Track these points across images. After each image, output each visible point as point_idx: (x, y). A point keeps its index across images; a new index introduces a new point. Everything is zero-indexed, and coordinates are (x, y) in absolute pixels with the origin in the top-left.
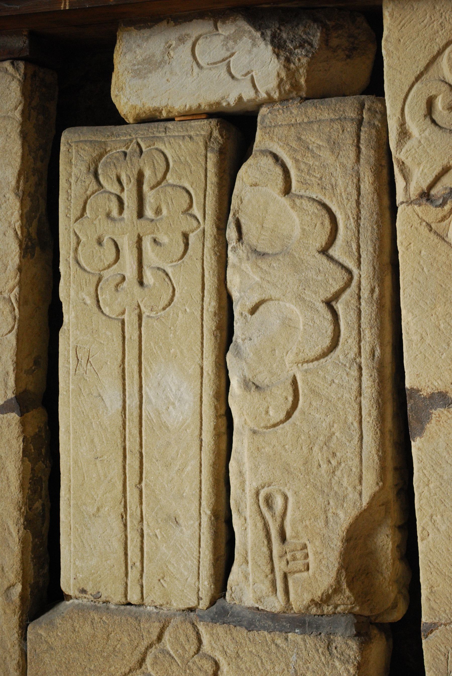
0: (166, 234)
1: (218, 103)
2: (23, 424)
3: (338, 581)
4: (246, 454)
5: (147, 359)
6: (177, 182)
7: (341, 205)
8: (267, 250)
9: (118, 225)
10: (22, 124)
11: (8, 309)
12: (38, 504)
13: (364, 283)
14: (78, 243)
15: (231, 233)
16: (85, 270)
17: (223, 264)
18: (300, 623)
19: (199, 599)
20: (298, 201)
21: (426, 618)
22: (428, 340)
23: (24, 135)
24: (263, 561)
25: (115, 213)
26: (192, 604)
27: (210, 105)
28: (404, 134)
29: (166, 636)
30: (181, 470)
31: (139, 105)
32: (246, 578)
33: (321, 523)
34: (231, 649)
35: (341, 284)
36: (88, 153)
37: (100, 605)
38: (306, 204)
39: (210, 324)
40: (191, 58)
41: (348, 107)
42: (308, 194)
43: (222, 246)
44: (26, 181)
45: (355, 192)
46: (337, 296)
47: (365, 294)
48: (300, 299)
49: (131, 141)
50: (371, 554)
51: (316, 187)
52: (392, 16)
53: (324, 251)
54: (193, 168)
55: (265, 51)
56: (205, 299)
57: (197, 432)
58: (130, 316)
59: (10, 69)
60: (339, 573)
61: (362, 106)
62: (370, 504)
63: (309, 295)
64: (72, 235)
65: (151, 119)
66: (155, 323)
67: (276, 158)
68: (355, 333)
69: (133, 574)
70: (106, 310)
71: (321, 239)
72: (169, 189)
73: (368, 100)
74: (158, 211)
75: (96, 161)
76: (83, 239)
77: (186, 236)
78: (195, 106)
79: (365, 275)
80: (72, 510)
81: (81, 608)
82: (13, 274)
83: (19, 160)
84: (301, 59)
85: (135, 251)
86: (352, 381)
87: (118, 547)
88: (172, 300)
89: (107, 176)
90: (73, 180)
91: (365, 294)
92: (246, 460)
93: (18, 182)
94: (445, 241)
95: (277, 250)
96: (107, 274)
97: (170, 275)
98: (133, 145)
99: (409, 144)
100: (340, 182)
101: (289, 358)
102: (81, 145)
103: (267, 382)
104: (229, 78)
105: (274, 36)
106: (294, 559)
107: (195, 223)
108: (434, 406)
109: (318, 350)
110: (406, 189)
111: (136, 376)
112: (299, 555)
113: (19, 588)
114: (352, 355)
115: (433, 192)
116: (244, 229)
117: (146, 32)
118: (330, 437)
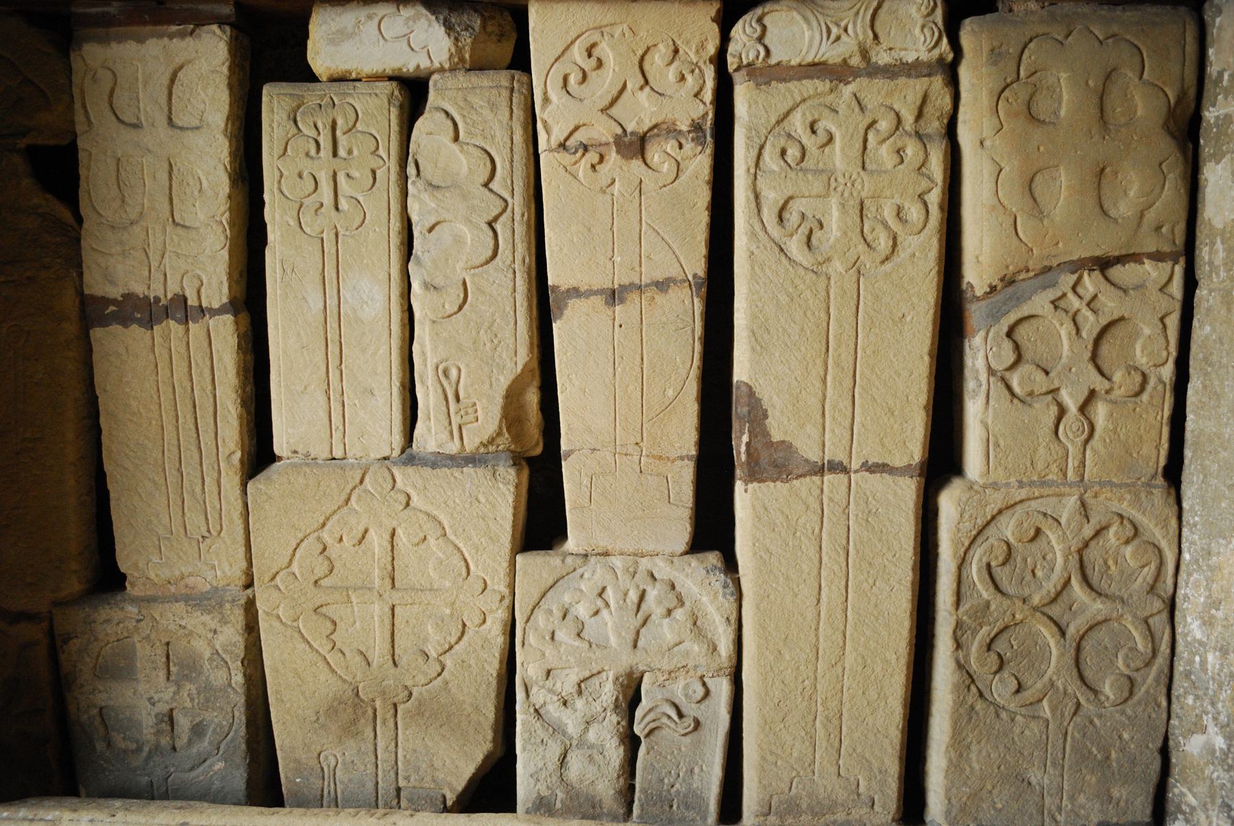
2: (236, 323)
3: (500, 428)
4: (427, 338)
9: (316, 162)
10: (229, 78)
11: (220, 229)
12: (248, 389)
14: (281, 176)
15: (411, 170)
17: (405, 194)
18: (472, 460)
19: (392, 449)
20: (465, 147)
21: (564, 447)
22: (565, 251)
23: (231, 87)
24: (443, 417)
25: (313, 152)
26: (386, 454)
28: (546, 100)
29: (367, 479)
30: (375, 353)
31: (333, 67)
32: (429, 430)
33: (487, 386)
34: (420, 483)
36: (288, 104)
37: (311, 461)
39: (395, 240)
41: (503, 77)
42: (473, 141)
43: (404, 178)
44: (233, 125)
46: (496, 219)
47: (517, 217)
48: (468, 221)
50: (522, 406)
52: (537, 12)
53: (486, 185)
55: (439, 31)
59: (218, 31)
60: (501, 421)
61: (513, 78)
62: (523, 370)
63: (475, 218)
65: (340, 79)
67: (447, 113)
68: (510, 246)
69: (337, 435)
70: (307, 230)
71: (484, 177)
73: (518, 74)
74: (350, 152)
75: (295, 111)
76: (286, 173)
77: (374, 172)
78: (380, 71)
79: (518, 203)
80: (283, 390)
81: (294, 466)
82: (224, 201)
83: (227, 107)
84: (467, 39)
85: (332, 183)
87: (323, 415)
88: (363, 222)
89: (304, 122)
91: (517, 217)
92: (427, 342)
93: (226, 125)
95: (449, 184)
96: (307, 202)
98: (327, 99)
99: (550, 108)
100: (498, 134)
105: (445, 20)
106: (467, 414)
107: (382, 163)
108: (569, 297)
109: (483, 259)
110: (548, 140)
112: (470, 410)
113: (239, 454)
114: (508, 262)
116: (421, 168)
117: (339, 9)
118: (492, 324)
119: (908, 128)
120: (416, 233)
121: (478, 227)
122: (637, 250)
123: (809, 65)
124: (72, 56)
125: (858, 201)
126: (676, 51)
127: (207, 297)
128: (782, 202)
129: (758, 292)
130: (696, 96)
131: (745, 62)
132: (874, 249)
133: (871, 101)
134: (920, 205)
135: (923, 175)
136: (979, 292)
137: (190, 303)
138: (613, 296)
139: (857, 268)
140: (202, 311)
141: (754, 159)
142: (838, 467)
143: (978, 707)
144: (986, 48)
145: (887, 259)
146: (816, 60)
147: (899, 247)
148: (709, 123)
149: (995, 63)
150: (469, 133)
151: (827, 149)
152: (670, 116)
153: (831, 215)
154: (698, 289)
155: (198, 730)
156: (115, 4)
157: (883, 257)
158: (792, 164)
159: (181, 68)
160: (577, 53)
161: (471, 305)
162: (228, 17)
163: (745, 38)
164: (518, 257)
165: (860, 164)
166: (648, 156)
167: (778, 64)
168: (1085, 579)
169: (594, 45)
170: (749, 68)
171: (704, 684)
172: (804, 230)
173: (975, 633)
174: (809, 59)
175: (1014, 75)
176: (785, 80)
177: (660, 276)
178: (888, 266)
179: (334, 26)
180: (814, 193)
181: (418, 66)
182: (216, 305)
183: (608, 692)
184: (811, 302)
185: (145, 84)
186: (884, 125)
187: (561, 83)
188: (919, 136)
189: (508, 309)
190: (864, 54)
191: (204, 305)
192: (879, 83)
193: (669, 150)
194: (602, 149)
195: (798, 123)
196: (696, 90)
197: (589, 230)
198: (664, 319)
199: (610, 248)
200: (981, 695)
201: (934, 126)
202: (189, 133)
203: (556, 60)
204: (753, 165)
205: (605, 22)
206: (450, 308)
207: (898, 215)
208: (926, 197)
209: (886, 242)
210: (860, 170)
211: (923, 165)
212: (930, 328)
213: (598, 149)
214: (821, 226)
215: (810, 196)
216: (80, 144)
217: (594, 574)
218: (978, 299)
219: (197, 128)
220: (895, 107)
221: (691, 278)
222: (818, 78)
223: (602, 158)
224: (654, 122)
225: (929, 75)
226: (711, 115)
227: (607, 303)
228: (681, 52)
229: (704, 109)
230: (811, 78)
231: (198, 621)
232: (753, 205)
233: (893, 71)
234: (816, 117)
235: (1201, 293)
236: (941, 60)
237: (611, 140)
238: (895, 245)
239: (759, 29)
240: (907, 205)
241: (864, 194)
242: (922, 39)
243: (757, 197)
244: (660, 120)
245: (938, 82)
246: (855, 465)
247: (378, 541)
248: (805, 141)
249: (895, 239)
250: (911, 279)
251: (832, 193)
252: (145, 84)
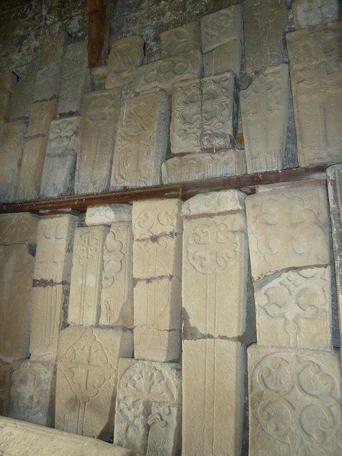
18: (112, 327)
37: (75, 326)
55: (112, 213)
56: (309, 270)
94: (325, 124)
138: (149, 281)
142: (210, 336)
143: (261, 434)
155: (38, 403)
160: (142, 216)
168: (301, 387)
170: (187, 217)
171: (170, 409)
173: (259, 402)
183: (141, 407)
200: (262, 429)
217: (139, 365)
231: (43, 369)
235: (287, 72)
246: (216, 337)
247: (87, 349)
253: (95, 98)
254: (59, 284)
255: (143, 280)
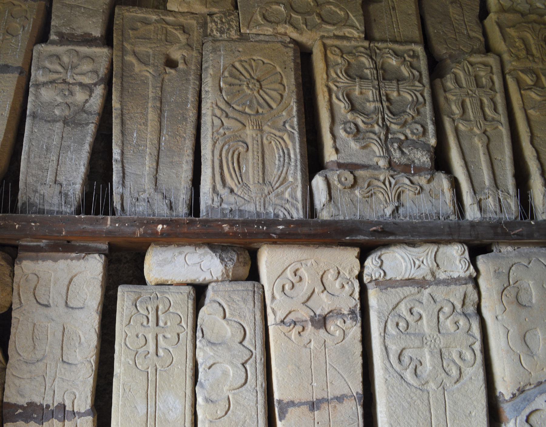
0: (170, 333)
1: (195, 280)
5: (159, 390)
6: (175, 311)
7: (248, 324)
8: (215, 342)
9: (147, 329)
13: (258, 356)
15: (199, 334)
16: (129, 348)
20: (230, 322)
22: (286, 380)
25: (145, 323)
27: (192, 281)
28: (273, 298)
31: (159, 278)
35: (249, 357)
36: (133, 296)
38: (233, 323)
39: (189, 373)
40: (184, 261)
41: (249, 285)
42: (233, 319)
43: (195, 338)
45: (253, 319)
46: (246, 362)
48: (231, 363)
49: (153, 292)
51: (237, 317)
53: (241, 343)
54: (182, 306)
55: (217, 261)
57: (183, 423)
58: (151, 369)
63: (235, 361)
64: (123, 333)
66: (164, 373)
67: (220, 304)
68: (255, 377)
70: (140, 367)
72: (171, 314)
74: (166, 324)
75: (136, 300)
76: (129, 334)
77: (178, 335)
79: (258, 353)
84: (230, 265)
85: (155, 341)
86: (254, 398)
89: (141, 306)
90: (125, 308)
93: (98, 307)
95: (220, 342)
97: (171, 352)
99: (275, 302)
100: (247, 315)
101: (225, 388)
102: (129, 293)
103: (215, 399)
104: (200, 270)
105: (220, 256)
107: (183, 330)
111: (154, 397)
114: (254, 386)
115: (285, 321)
117: (164, 249)
119: (459, 311)
120: (201, 370)
121: (236, 366)
122: (325, 379)
123: (406, 280)
124: (16, 266)
125: (439, 350)
126: (339, 273)
127: (78, 405)
128: (399, 351)
129: (392, 402)
130: (351, 295)
131: (374, 278)
132: (450, 376)
133: (438, 298)
134: (471, 351)
135: (470, 335)
136: (507, 398)
137: (67, 409)
138: (313, 406)
139: (442, 386)
140: (74, 414)
141: (383, 329)
144: (492, 270)
145: (458, 381)
146: (410, 277)
147: (463, 374)
148: (358, 309)
149: (497, 278)
150: (232, 314)
151: (419, 323)
152: (338, 306)
153: (425, 357)
154: (359, 401)
156: (44, 241)
157: (456, 380)
158: (403, 331)
159: (75, 276)
160: (289, 273)
161: (233, 412)
162: (105, 250)
163: (373, 267)
164: (259, 383)
165: (438, 330)
166: (328, 327)
167: (390, 279)
169: (297, 270)
170: (377, 282)
172: (412, 366)
174: (406, 277)
175: (508, 283)
176: (394, 287)
177: (338, 393)
178: (458, 385)
179: (161, 257)
180: (416, 345)
181: (205, 279)
182: (83, 410)
184: (420, 406)
185: (55, 283)
186: (447, 309)
187: (281, 289)
188: (465, 315)
189: (253, 413)
190: (433, 274)
191: (75, 411)
192: (442, 288)
193: (338, 324)
194: (304, 324)
195: (403, 309)
196: (350, 292)
197: (299, 368)
198: (342, 419)
199: (310, 378)
201: (471, 309)
202: (77, 311)
203: (278, 277)
204: (383, 331)
205: (303, 258)
206: (220, 413)
207: (460, 356)
208: (473, 347)
209: (456, 372)
210: (438, 333)
211: (469, 330)
212: (486, 419)
213: (301, 324)
214: (421, 364)
215: (414, 348)
216: (14, 314)
218: (507, 401)
219: (82, 308)
220: (451, 300)
221: (355, 395)
222: (411, 286)
223: (304, 329)
224: (330, 309)
225: (466, 284)
226: (359, 306)
227: (310, 410)
228: (341, 273)
229: (355, 302)
230: (407, 286)
232: (385, 353)
233: (448, 282)
234: (412, 305)
236: (470, 276)
237: (308, 319)
238: (461, 373)
239: (380, 262)
240: (464, 351)
241: (441, 346)
242: (461, 266)
243: (386, 348)
244: (333, 308)
245: (470, 287)
248: (407, 318)
249: (460, 370)
250: (472, 392)
251: (425, 346)
252: (55, 283)
253: (146, 22)
254: (81, 415)
255: (300, 404)
